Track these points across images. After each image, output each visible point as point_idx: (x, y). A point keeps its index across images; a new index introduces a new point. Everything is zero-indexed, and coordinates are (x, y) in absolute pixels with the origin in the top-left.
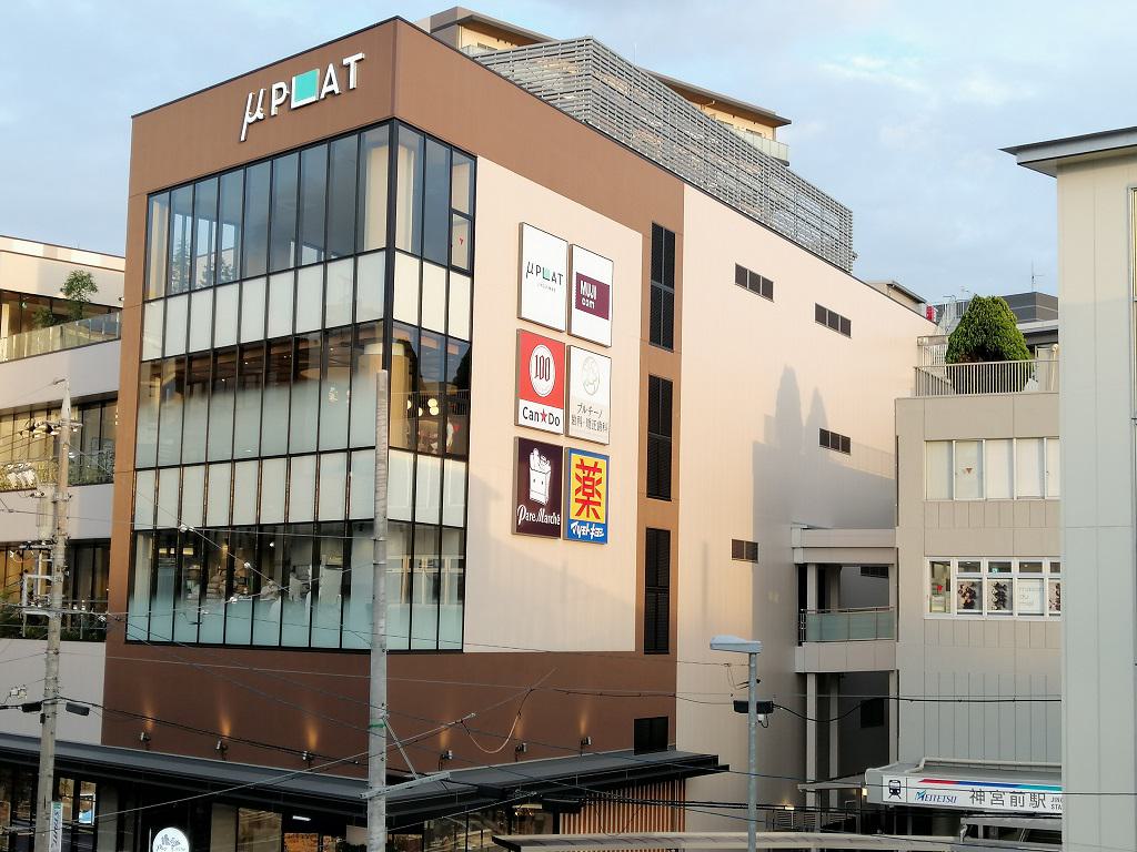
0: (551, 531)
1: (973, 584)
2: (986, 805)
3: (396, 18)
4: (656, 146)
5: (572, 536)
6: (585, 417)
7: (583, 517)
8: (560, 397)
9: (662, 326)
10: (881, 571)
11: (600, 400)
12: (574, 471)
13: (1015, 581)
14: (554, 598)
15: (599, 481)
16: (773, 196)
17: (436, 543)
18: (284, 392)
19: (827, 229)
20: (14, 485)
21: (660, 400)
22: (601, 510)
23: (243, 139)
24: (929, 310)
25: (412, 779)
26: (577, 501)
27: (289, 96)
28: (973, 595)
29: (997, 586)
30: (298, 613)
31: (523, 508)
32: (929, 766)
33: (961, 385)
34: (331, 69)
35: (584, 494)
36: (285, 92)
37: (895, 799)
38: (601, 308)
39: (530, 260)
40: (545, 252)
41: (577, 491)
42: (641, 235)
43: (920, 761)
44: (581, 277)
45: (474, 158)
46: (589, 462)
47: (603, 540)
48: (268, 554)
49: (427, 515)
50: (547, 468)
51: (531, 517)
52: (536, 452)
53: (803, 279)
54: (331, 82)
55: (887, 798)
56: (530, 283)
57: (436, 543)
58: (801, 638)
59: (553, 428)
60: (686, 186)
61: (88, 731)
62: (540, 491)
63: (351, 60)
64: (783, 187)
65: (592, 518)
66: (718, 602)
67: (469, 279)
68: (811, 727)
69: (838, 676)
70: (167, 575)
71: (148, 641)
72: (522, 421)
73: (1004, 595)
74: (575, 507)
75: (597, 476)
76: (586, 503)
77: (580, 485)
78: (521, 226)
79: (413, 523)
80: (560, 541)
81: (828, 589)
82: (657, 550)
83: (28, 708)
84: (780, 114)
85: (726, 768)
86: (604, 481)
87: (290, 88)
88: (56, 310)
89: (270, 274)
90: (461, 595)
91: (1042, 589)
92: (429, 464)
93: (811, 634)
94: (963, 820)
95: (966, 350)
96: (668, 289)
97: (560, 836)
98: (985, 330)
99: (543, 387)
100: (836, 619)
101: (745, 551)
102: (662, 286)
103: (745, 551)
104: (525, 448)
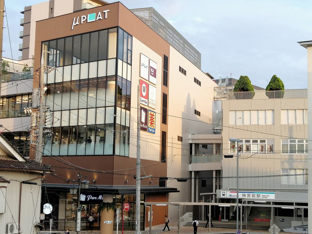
1: (241, 146)
3: (119, 2)
4: (160, 33)
5: (149, 132)
7: (151, 127)
8: (147, 97)
9: (165, 82)
13: (251, 145)
14: (147, 147)
18: (68, 94)
21: (165, 98)
22: (154, 125)
23: (72, 29)
26: (150, 123)
27: (87, 19)
28: (241, 148)
29: (247, 146)
33: (237, 97)
34: (100, 13)
35: (151, 121)
36: (86, 18)
37: (224, 197)
38: (155, 76)
39: (140, 63)
40: (145, 61)
43: (228, 189)
44: (151, 67)
46: (152, 113)
47: (154, 133)
49: (123, 124)
53: (192, 71)
54: (99, 16)
56: (142, 67)
59: (145, 104)
62: (143, 120)
63: (106, 11)
66: (175, 151)
71: (51, 156)
73: (248, 148)
74: (149, 124)
75: (153, 117)
76: (152, 123)
81: (194, 149)
82: (164, 135)
85: (179, 191)
86: (155, 118)
87: (87, 17)
89: (90, 62)
90: (129, 144)
91: (258, 147)
95: (239, 89)
98: (244, 84)
99: (144, 94)
100: (200, 157)
101: (180, 139)
102: (165, 70)
103: (180, 139)
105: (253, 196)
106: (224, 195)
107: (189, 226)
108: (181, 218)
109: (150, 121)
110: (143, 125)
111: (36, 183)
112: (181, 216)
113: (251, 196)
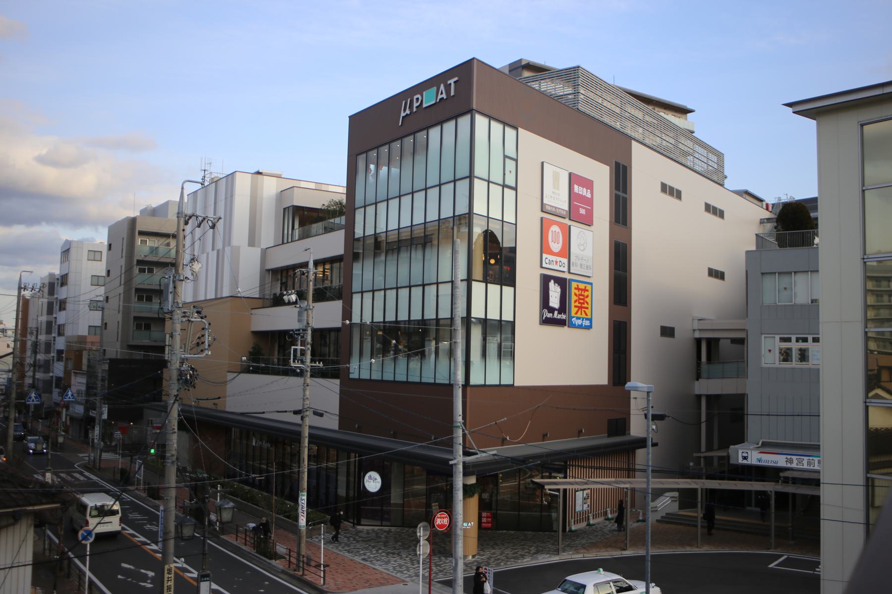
0: (561, 323)
2: (794, 465)
6: (579, 263)
7: (579, 315)
8: (566, 251)
10: (741, 341)
11: (588, 253)
12: (573, 291)
14: (558, 359)
15: (587, 296)
16: (682, 149)
17: (501, 331)
19: (710, 163)
20: (287, 301)
24: (767, 205)
25: (476, 454)
26: (576, 307)
30: (415, 364)
31: (546, 311)
32: (764, 444)
34: (442, 87)
37: (745, 462)
41: (575, 301)
42: (608, 168)
45: (516, 129)
46: (582, 286)
47: (589, 327)
48: (411, 337)
49: (493, 315)
50: (558, 289)
51: (550, 315)
52: (552, 281)
55: (741, 461)
57: (501, 331)
58: (698, 377)
59: (561, 269)
60: (633, 142)
61: (331, 422)
62: (554, 302)
63: (452, 81)
64: (690, 144)
65: (584, 315)
67: (514, 192)
68: (703, 426)
69: (718, 397)
70: (492, 347)
72: (544, 265)
74: (574, 310)
76: (580, 308)
77: (576, 298)
78: (542, 163)
79: (501, 321)
80: (566, 327)
83: (296, 412)
84: (689, 107)
88: (321, 215)
92: (494, 289)
93: (704, 374)
94: (781, 474)
96: (625, 195)
97: (568, 480)
99: (556, 247)
102: (621, 194)
104: (546, 280)
105: (809, 464)
106: (745, 458)
107: (667, 523)
108: (652, 504)
109: (577, 304)
110: (556, 312)
111: (733, 345)
112: (653, 501)
113: (805, 462)
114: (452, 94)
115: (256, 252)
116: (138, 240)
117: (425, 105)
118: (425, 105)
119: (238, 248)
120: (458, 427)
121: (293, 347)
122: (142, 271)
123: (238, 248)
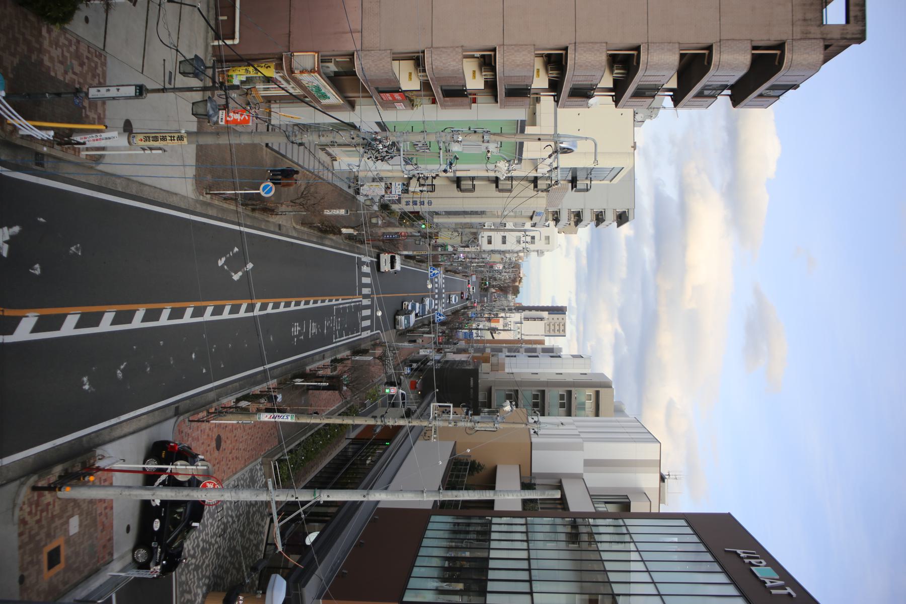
63: (789, 590)
114: (774, 592)
115: (579, 468)
116: (590, 392)
117: (753, 568)
118: (753, 568)
119: (582, 449)
120: (314, 495)
121: (451, 405)
122: (562, 397)
123: (582, 449)
